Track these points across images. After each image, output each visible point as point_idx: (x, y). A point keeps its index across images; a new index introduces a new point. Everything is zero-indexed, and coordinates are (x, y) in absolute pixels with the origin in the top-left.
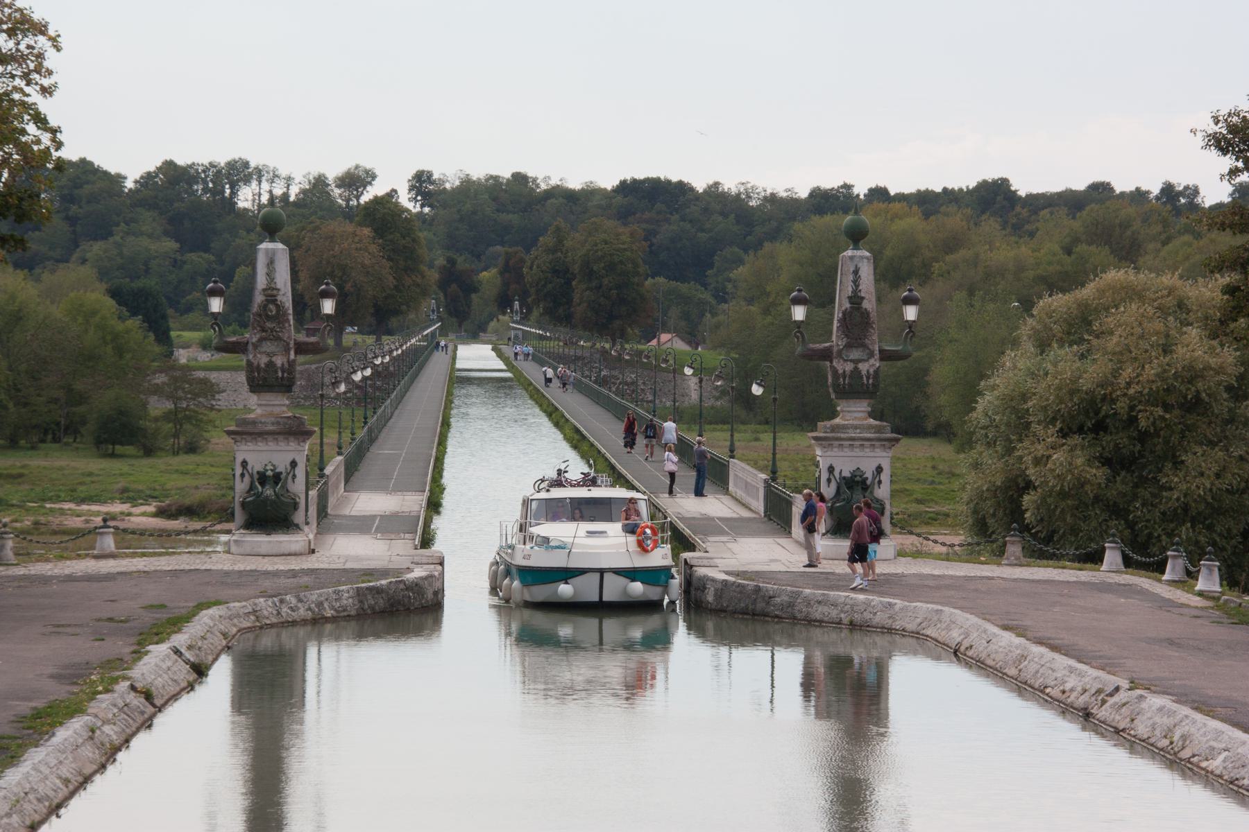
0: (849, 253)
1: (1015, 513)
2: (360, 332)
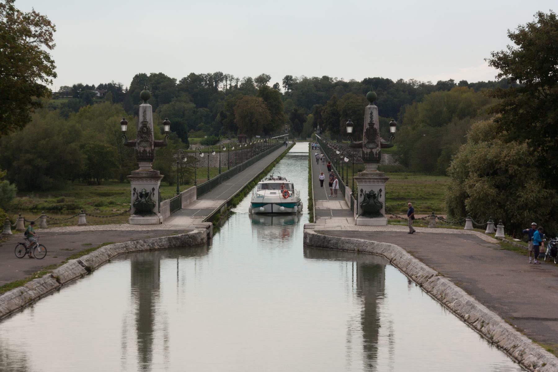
0: (369, 106)
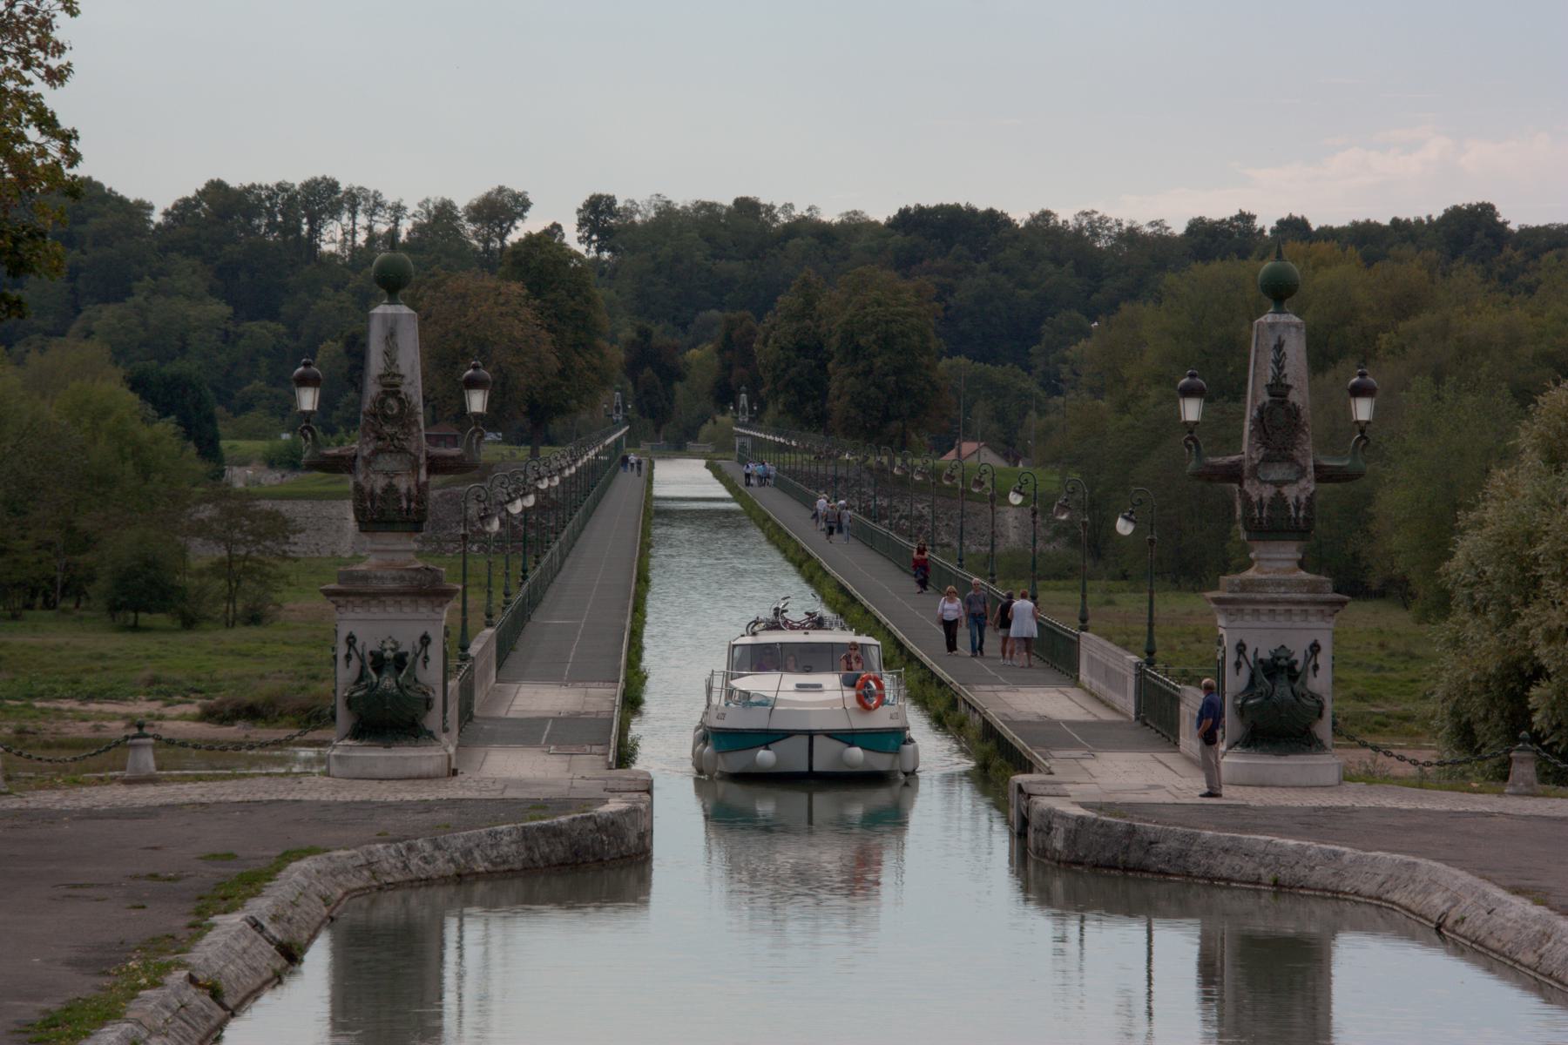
0: (1268, 318)
1: (1517, 721)
2: (506, 441)
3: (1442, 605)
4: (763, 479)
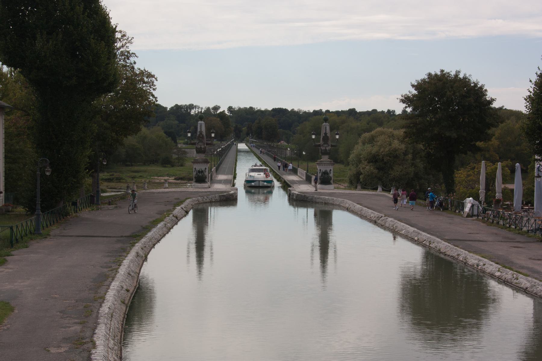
1: (358, 180)
3: (348, 164)
4: (254, 146)
